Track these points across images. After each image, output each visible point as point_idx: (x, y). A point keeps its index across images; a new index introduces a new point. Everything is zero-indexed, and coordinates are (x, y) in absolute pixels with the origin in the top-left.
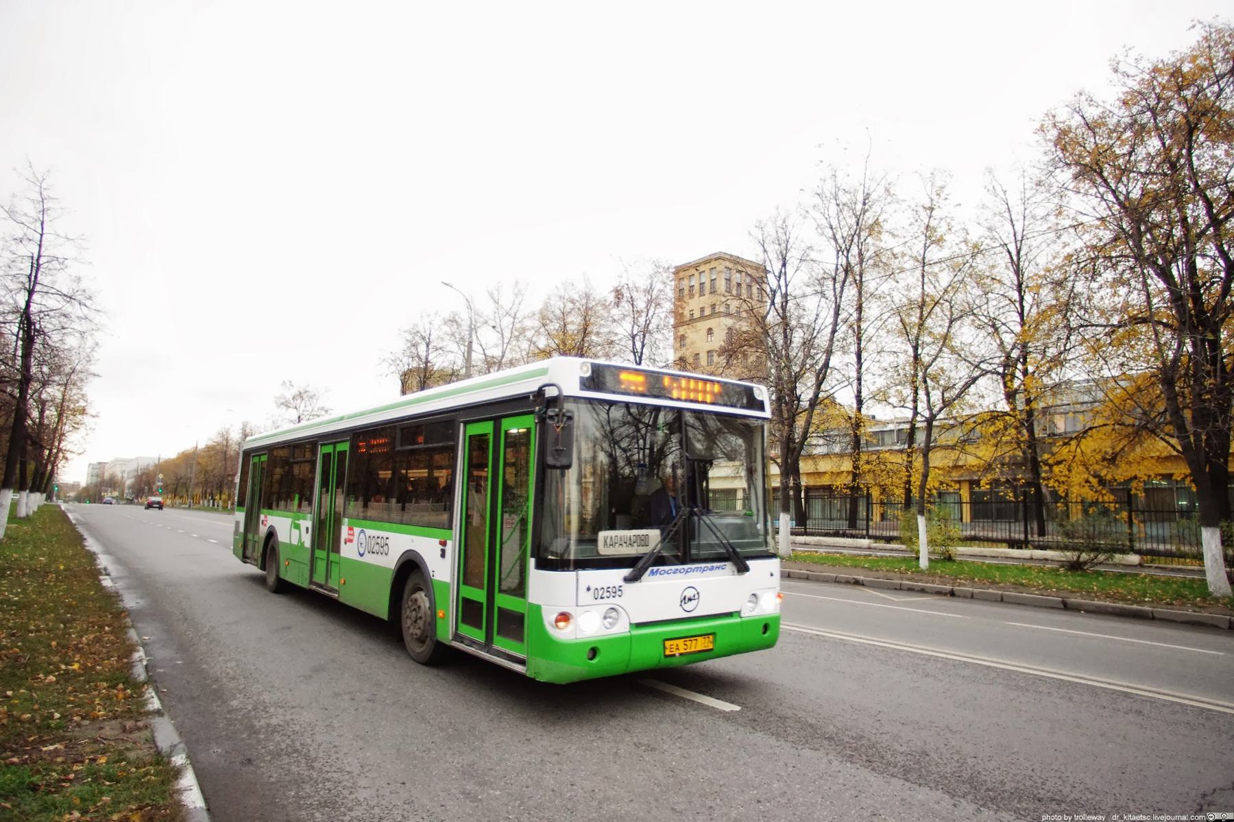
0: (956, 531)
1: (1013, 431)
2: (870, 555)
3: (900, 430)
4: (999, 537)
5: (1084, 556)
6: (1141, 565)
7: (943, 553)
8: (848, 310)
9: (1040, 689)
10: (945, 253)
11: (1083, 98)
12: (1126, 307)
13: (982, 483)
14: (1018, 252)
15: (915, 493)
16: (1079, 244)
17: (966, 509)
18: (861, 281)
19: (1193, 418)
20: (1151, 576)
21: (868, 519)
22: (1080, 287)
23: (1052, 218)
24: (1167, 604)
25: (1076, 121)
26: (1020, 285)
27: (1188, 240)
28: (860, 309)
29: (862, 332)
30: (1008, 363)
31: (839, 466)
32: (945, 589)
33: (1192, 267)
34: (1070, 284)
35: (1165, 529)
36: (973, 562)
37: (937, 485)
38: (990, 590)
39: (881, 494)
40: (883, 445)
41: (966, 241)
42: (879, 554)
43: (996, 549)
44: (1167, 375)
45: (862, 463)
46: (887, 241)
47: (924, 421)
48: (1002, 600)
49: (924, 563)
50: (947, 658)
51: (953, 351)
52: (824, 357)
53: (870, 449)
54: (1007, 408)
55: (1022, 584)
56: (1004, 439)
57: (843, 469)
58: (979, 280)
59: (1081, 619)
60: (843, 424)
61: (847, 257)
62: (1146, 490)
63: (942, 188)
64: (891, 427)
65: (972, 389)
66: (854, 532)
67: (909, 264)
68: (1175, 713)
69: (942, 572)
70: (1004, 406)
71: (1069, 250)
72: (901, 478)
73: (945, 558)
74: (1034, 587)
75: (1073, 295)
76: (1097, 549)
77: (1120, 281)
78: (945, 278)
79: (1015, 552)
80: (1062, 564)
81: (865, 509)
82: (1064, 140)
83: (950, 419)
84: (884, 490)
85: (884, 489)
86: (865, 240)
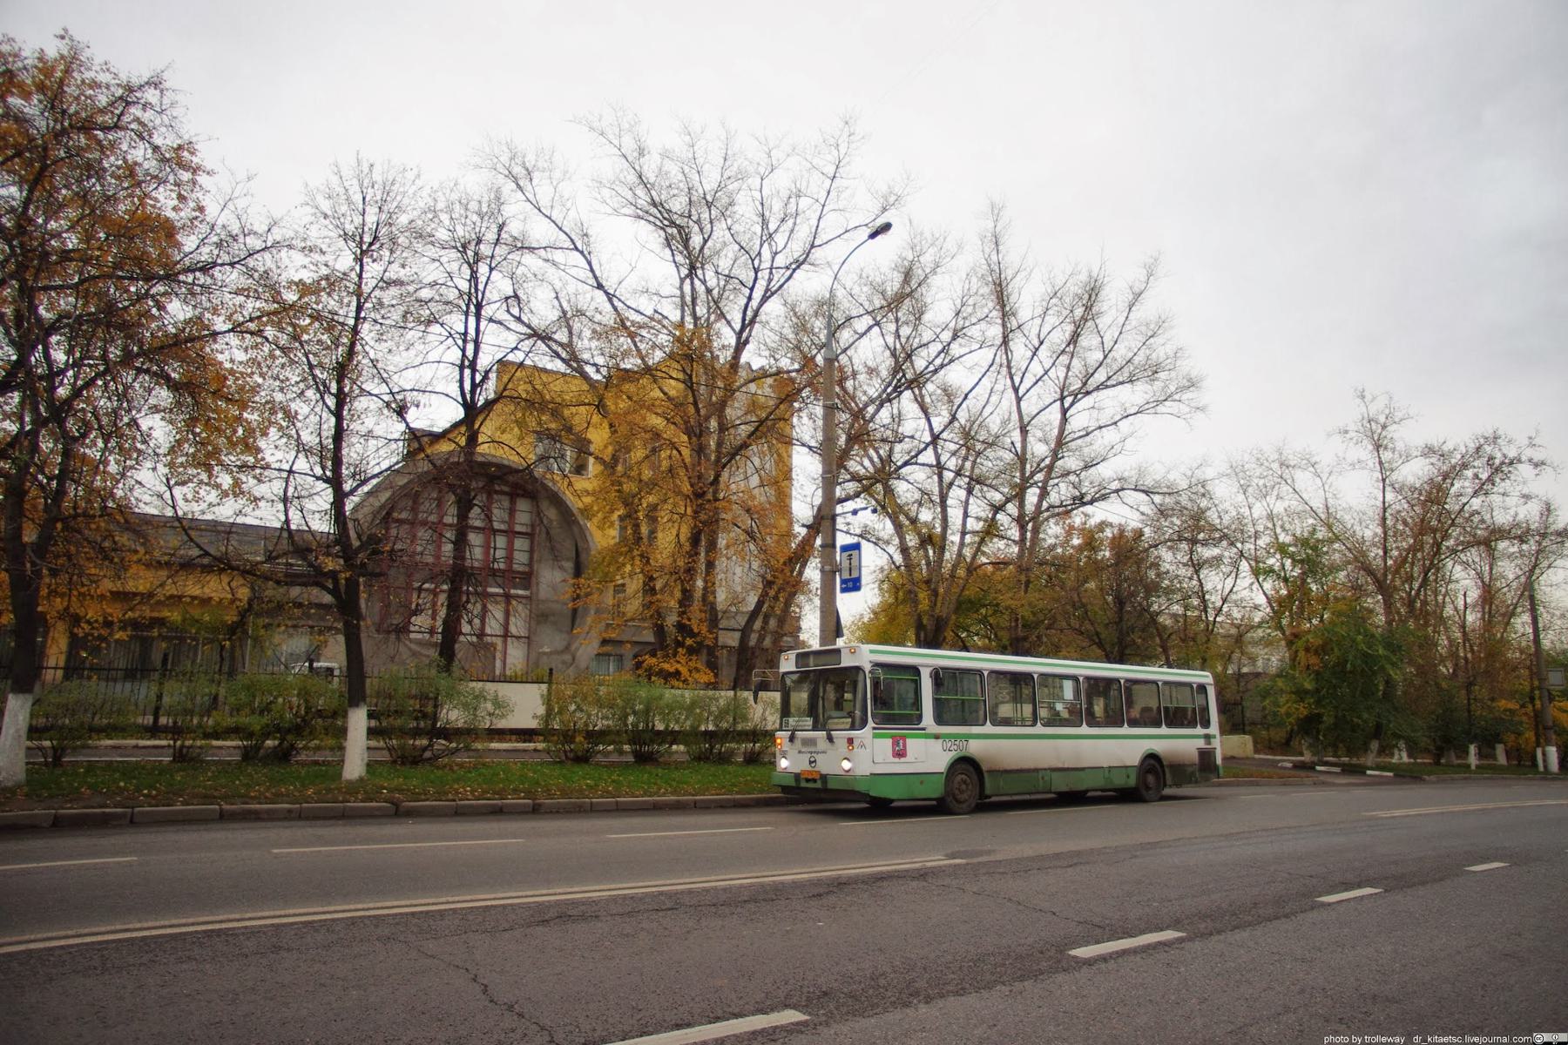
38: (36, 811)
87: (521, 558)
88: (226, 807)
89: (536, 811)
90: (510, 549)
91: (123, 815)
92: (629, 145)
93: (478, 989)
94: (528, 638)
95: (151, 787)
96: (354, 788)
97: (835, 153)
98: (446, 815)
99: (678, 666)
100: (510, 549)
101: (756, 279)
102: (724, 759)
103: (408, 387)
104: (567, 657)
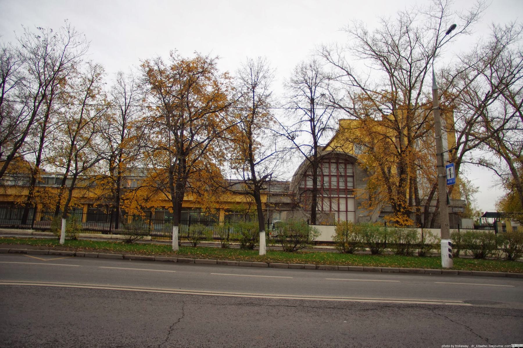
0: (79, 226)
1: (110, 184)
2: (32, 238)
3: (57, 178)
4: (99, 229)
5: (133, 237)
6: (151, 240)
7: (72, 236)
8: (40, 116)
9: (114, 296)
10: (95, 102)
11: (160, 60)
12: (160, 142)
13: (94, 205)
14: (126, 111)
15: (62, 209)
16: (149, 115)
17: (85, 216)
18: (50, 103)
19: (177, 187)
20: (155, 244)
21: (34, 219)
22: (146, 131)
23: (141, 102)
24: (160, 254)
25: (156, 68)
26: (124, 124)
27: (191, 121)
28: (47, 117)
29: (46, 128)
30: (113, 156)
31: (21, 192)
32: (72, 253)
33: (182, 133)
34: (143, 129)
35: (160, 227)
36: (86, 240)
37: (73, 205)
38: (93, 253)
39: (43, 207)
40: (48, 184)
41: (105, 100)
42: (38, 237)
43: (97, 234)
44: (171, 170)
45: (35, 191)
46: (68, 89)
47: (73, 175)
48: (98, 257)
49: (62, 241)
50: (71, 287)
51: (91, 146)
52: (21, 136)
53: (40, 185)
54: (109, 175)
55: (107, 250)
56: (107, 187)
57: (22, 194)
58: (108, 118)
59: (130, 263)
60: (27, 172)
61: (45, 91)
62: (155, 212)
63: (99, 74)
64: (54, 176)
65: (96, 164)
66: (24, 226)
67: (76, 102)
68: (162, 297)
69: (71, 245)
70: (108, 174)
71: (144, 115)
72: (55, 201)
73: (73, 239)
74: (112, 250)
75: (143, 134)
76: (137, 234)
77: (160, 133)
78: (93, 114)
79: (105, 236)
80: (124, 240)
81: (33, 215)
82: (150, 72)
83: (84, 176)
84: (45, 206)
85: (44, 205)
86: (56, 85)
87: (350, 185)
88: (219, 260)
89: (317, 268)
90: (330, 182)
91: (192, 261)
92: (360, 32)
93: (478, 337)
94: (355, 212)
95: (204, 254)
96: (263, 258)
97: (440, 6)
98: (285, 268)
99: (398, 219)
100: (330, 182)
101: (411, 67)
102: (409, 254)
103: (294, 130)
104: (369, 218)
